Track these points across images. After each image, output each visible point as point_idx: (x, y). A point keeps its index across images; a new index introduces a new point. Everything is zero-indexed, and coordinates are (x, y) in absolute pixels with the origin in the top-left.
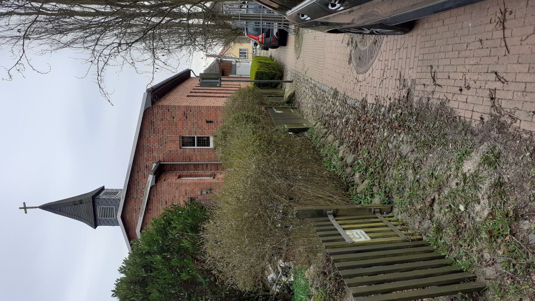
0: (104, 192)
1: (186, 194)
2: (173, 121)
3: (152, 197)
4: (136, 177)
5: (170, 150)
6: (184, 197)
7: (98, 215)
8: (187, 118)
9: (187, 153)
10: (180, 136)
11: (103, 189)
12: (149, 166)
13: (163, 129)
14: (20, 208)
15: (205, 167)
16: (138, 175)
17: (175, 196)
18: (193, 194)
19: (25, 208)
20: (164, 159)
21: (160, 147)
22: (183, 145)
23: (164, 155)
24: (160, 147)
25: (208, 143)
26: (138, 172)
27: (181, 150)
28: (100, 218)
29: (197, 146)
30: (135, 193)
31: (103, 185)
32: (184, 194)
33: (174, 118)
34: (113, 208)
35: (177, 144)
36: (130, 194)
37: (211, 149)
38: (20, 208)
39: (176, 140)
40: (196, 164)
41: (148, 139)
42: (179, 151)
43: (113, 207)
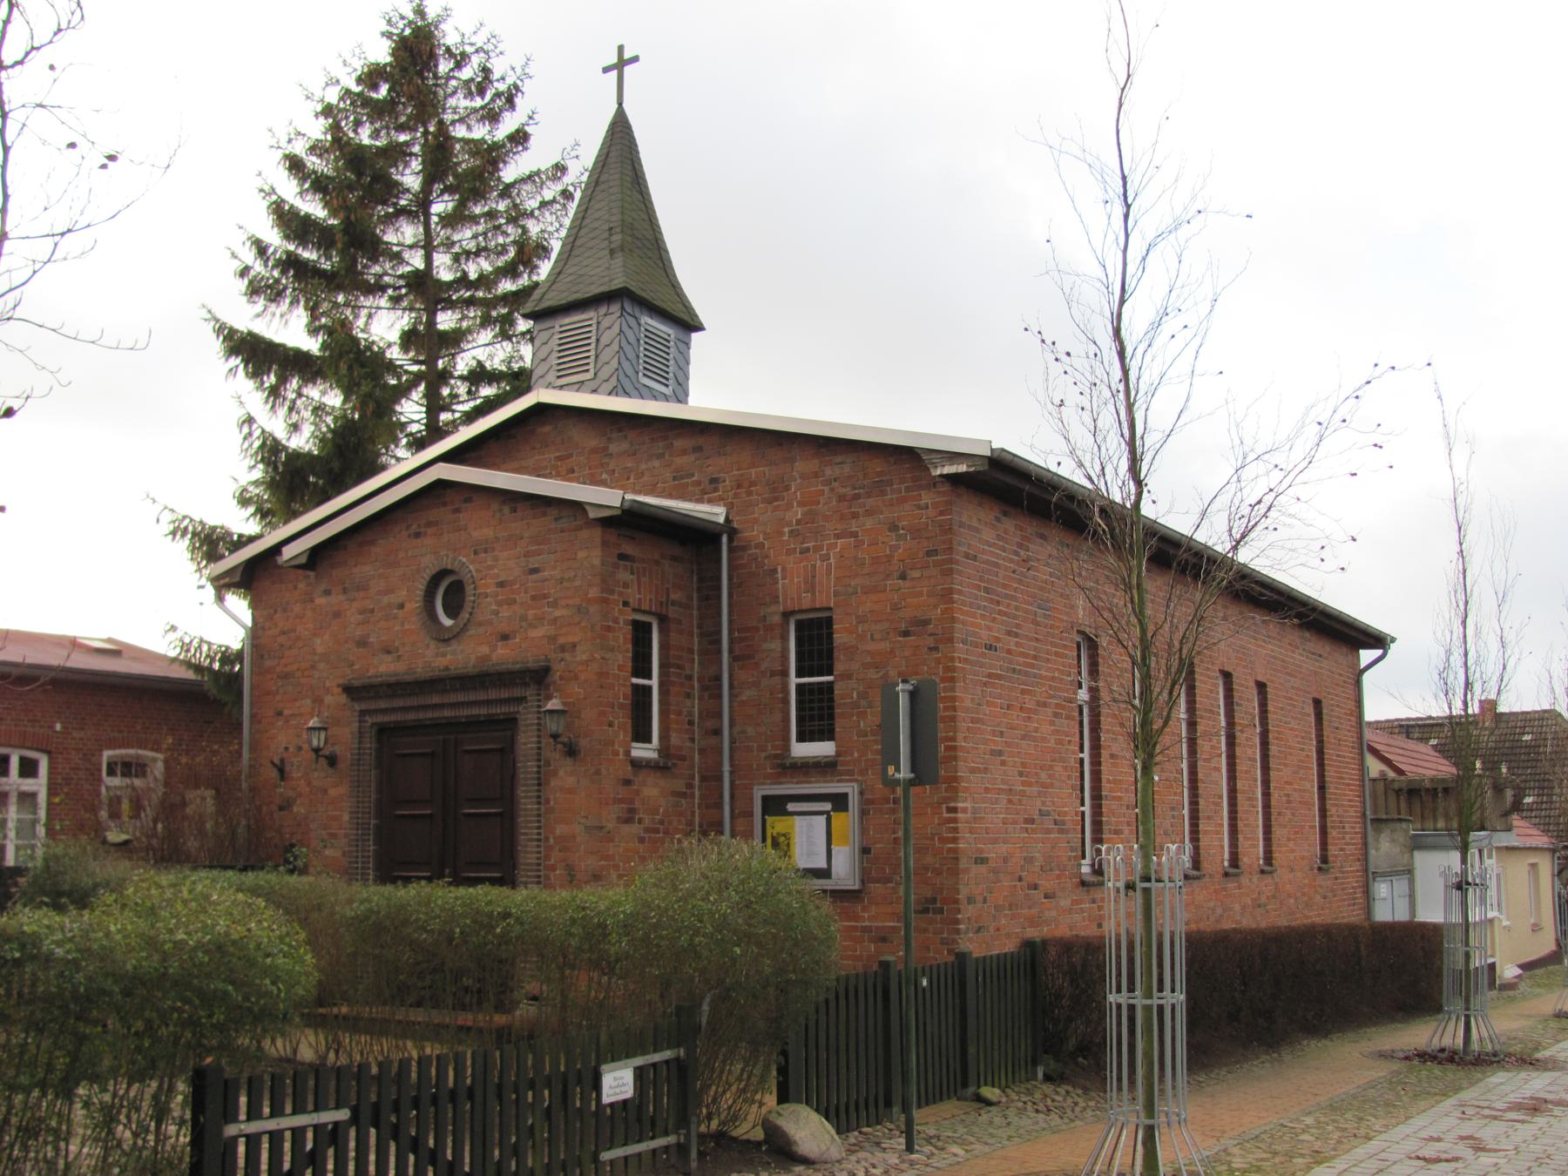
0: (670, 331)
1: (563, 649)
2: (888, 577)
3: (554, 512)
4: (679, 444)
5: (775, 571)
6: (552, 639)
7: (567, 321)
8: (906, 634)
9: (765, 646)
10: (830, 609)
11: (688, 324)
12: (716, 490)
13: (854, 534)
14: (621, 49)
15: (710, 724)
16: (684, 452)
17: (555, 604)
18: (561, 678)
19: (621, 64)
20: (744, 548)
21: (786, 530)
22: (800, 626)
23: (757, 546)
24: (786, 530)
25: (812, 732)
26: (698, 449)
27: (777, 619)
28: (557, 327)
29: (800, 687)
30: (624, 446)
31: (705, 326)
32: (561, 640)
33: (903, 577)
34: (587, 371)
35: (800, 598)
36: (620, 430)
37: (786, 747)
38: (621, 49)
39: (814, 594)
40: (720, 687)
41: (816, 475)
42: (773, 608)
43: (592, 371)
